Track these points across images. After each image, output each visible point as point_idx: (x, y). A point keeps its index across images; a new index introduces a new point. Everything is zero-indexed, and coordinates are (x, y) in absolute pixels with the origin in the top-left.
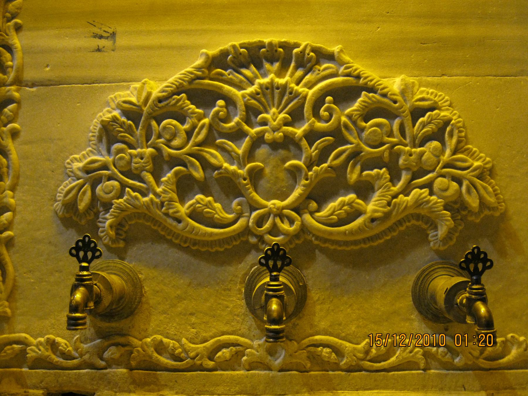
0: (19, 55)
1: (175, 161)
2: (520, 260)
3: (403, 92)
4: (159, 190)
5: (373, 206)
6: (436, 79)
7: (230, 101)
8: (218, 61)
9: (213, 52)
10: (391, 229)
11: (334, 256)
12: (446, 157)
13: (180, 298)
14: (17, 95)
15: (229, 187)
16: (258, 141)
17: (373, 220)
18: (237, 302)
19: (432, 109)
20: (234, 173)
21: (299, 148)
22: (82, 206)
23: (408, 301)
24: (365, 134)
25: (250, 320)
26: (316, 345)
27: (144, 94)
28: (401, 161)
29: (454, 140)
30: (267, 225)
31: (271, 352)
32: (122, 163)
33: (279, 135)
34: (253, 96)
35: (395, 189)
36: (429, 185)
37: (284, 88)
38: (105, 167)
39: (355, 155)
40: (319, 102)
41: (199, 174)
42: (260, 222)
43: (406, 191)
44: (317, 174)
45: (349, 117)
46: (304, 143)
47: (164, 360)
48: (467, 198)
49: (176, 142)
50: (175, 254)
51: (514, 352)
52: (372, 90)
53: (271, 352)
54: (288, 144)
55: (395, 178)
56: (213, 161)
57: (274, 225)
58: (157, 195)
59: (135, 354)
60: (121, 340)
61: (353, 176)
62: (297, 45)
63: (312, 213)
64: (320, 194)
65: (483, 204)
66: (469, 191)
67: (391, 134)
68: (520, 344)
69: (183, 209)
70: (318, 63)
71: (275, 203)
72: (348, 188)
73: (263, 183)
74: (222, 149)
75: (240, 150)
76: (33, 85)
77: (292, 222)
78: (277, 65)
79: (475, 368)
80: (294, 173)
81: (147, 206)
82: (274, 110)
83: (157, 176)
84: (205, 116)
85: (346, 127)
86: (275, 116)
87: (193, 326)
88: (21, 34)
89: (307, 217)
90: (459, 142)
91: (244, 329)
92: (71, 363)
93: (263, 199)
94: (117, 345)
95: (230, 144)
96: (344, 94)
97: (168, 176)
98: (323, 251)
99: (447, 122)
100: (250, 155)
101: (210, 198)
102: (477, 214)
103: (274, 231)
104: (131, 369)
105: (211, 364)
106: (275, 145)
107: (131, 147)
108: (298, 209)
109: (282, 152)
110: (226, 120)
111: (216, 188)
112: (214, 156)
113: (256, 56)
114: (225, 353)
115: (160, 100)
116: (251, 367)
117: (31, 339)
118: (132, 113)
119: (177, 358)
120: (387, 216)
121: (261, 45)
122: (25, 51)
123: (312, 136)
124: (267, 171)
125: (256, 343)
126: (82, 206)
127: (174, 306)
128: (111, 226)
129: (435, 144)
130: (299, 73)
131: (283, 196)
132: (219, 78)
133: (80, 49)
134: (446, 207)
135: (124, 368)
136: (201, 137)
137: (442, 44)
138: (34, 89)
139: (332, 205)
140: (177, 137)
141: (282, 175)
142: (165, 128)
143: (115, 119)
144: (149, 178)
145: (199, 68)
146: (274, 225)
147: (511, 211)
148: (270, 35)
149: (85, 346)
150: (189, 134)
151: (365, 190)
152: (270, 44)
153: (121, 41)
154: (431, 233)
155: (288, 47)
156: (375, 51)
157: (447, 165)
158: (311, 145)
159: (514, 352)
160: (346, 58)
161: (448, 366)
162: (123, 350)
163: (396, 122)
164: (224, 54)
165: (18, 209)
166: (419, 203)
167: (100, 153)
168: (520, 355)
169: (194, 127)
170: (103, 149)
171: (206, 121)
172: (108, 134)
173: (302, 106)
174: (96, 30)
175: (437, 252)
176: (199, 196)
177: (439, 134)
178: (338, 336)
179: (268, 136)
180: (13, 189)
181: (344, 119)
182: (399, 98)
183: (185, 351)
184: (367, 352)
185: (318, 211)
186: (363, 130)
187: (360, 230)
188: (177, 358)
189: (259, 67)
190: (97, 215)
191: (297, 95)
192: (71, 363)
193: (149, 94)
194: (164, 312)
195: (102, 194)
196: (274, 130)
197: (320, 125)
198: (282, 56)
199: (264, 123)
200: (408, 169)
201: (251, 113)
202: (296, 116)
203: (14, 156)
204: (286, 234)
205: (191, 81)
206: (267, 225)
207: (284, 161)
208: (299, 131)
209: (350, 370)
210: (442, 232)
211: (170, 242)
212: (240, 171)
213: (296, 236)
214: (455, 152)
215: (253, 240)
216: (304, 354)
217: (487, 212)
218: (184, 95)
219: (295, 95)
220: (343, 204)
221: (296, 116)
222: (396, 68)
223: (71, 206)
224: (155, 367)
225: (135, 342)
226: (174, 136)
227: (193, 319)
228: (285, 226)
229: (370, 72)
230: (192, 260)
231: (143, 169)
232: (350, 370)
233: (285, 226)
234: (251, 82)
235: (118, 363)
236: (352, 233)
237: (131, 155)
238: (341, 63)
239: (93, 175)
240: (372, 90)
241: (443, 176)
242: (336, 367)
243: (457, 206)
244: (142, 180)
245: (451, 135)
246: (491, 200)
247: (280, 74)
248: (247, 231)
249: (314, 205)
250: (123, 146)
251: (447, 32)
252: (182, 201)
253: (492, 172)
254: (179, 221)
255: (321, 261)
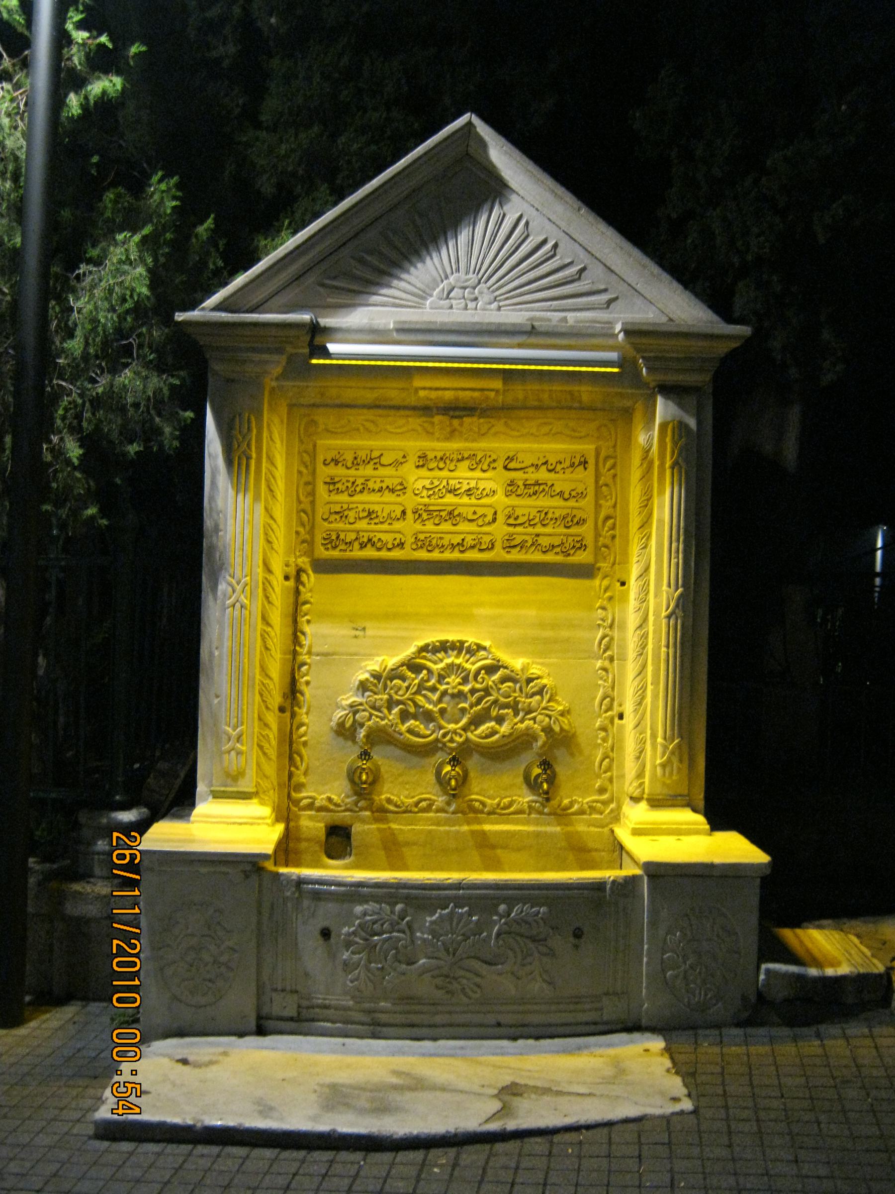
0: (309, 637)
1: (399, 703)
2: (581, 758)
3: (522, 670)
4: (391, 718)
5: (504, 729)
6: (541, 660)
7: (430, 671)
8: (424, 649)
9: (421, 643)
10: (513, 741)
11: (482, 754)
12: (544, 704)
13: (400, 775)
14: (308, 661)
15: (428, 717)
16: (444, 693)
17: (504, 736)
18: (431, 778)
19: (537, 678)
20: (431, 711)
21: (466, 698)
22: (348, 725)
23: (521, 779)
24: (501, 692)
25: (437, 787)
26: (472, 800)
27: (383, 667)
28: (520, 706)
29: (548, 695)
30: (448, 738)
31: (448, 804)
32: (371, 703)
33: (456, 691)
34: (443, 669)
35: (516, 720)
36: (534, 719)
37: (459, 666)
38: (361, 704)
39: (495, 702)
40: (477, 673)
41: (412, 710)
42: (444, 735)
43: (522, 721)
44: (475, 711)
45: (493, 682)
46: (469, 695)
47: (391, 808)
48: (553, 726)
49: (401, 693)
50: (398, 752)
51: (576, 807)
52: (506, 668)
53: (448, 804)
54: (460, 695)
55: (516, 714)
56: (420, 703)
57: (452, 738)
58: (390, 720)
59: (375, 804)
60: (368, 797)
61: (494, 713)
62: (467, 641)
63: (472, 732)
64: (476, 722)
65: (562, 729)
66: (554, 723)
67: (515, 691)
68: (579, 803)
69: (403, 728)
70: (478, 650)
71: (452, 726)
72: (490, 719)
73: (447, 716)
74: (425, 696)
75: (435, 697)
76: (318, 655)
77: (461, 736)
78: (456, 652)
79: (555, 814)
80: (463, 711)
81: (384, 726)
82: (453, 677)
83: (390, 709)
84: (416, 678)
85: (492, 688)
86: (454, 680)
87: (407, 790)
88: (311, 625)
89: (469, 734)
90: (551, 695)
91: (434, 791)
92: (339, 809)
93: (226, 284)
94: (365, 799)
95: (429, 694)
96: (491, 670)
97: (395, 710)
98: (477, 751)
99: (545, 686)
100: (440, 700)
101: (418, 723)
102: (559, 735)
103: (452, 740)
104: (373, 812)
105: (416, 810)
106: (453, 696)
107: (375, 693)
108: (465, 729)
109: (457, 700)
110: (428, 680)
111: (421, 717)
112: (420, 699)
113: (444, 647)
114: (424, 804)
115: (392, 670)
116: (437, 811)
117: (317, 796)
118: (377, 676)
119: (397, 806)
120: (511, 734)
121: (447, 641)
122: (312, 635)
123: (473, 691)
124: (449, 709)
125: (440, 799)
126: (348, 725)
127: (396, 779)
128: (364, 736)
129: (538, 697)
130: (468, 656)
131: (457, 722)
132: (424, 658)
133: (343, 636)
134: (542, 730)
135: (282, 874)
136: (414, 690)
137: (546, 641)
138: (318, 658)
139: (483, 728)
140: (401, 690)
141: (456, 711)
142: (394, 685)
143: (367, 680)
144: (385, 711)
145: (414, 654)
146: (452, 738)
147: (578, 733)
148: (452, 637)
149: (348, 800)
150: (408, 688)
151: (500, 720)
152: (453, 641)
153: (369, 632)
154: (534, 745)
155: (462, 643)
156: (511, 645)
157: (545, 708)
158: (472, 696)
159: (576, 807)
160: (493, 650)
161: (541, 813)
162: (368, 802)
163: (518, 686)
164: (427, 645)
165: (311, 725)
166: (528, 728)
167: (357, 696)
168: (579, 808)
169: (410, 685)
170: (360, 693)
171: (416, 681)
172: (363, 687)
173: (468, 675)
174: (354, 626)
175: (537, 754)
176: (412, 722)
177: (540, 692)
178: (484, 796)
179: (450, 691)
180: (307, 713)
181: (490, 683)
182: (520, 673)
183: (403, 803)
184: (498, 805)
185: (476, 729)
186: (500, 689)
187: (497, 741)
188: (397, 806)
189: (446, 652)
190: (355, 730)
191: (466, 670)
192: (339, 809)
193: (386, 667)
194: (392, 782)
195: (359, 720)
196: (454, 688)
197: (478, 686)
198: (458, 647)
199: (448, 683)
200: (523, 710)
201: (441, 678)
202: (465, 680)
203: (307, 695)
204: (458, 743)
205: (409, 660)
206: (448, 738)
207: (458, 704)
208: (466, 689)
209: (489, 813)
210: (540, 743)
211: (395, 745)
212: (435, 709)
213: (463, 743)
214: (549, 701)
215: (440, 745)
216: (465, 805)
217: (564, 734)
218: (405, 668)
219: (464, 670)
220: (488, 728)
221: (465, 680)
222: (518, 654)
223: (341, 725)
224: (387, 811)
225: (376, 798)
226: (399, 689)
227: (407, 786)
228: (457, 739)
229: (505, 657)
230: (408, 755)
231: (381, 707)
232: (489, 813)
233: (457, 739)
234: (441, 660)
235: (365, 809)
236: (492, 743)
237: (376, 700)
238: (490, 653)
239: (354, 709)
240: (506, 668)
241: (542, 714)
242: (482, 812)
243: (548, 730)
244: (381, 712)
245: (547, 693)
246: (566, 727)
247: (457, 656)
248: (437, 740)
249: (473, 727)
250: (371, 694)
251: (548, 633)
252: (403, 723)
253: (569, 712)
254: (401, 734)
255: (476, 757)
